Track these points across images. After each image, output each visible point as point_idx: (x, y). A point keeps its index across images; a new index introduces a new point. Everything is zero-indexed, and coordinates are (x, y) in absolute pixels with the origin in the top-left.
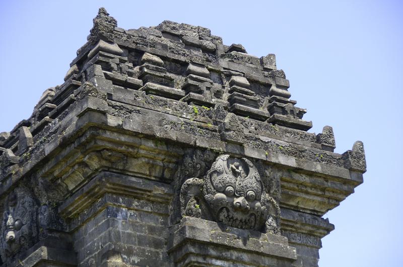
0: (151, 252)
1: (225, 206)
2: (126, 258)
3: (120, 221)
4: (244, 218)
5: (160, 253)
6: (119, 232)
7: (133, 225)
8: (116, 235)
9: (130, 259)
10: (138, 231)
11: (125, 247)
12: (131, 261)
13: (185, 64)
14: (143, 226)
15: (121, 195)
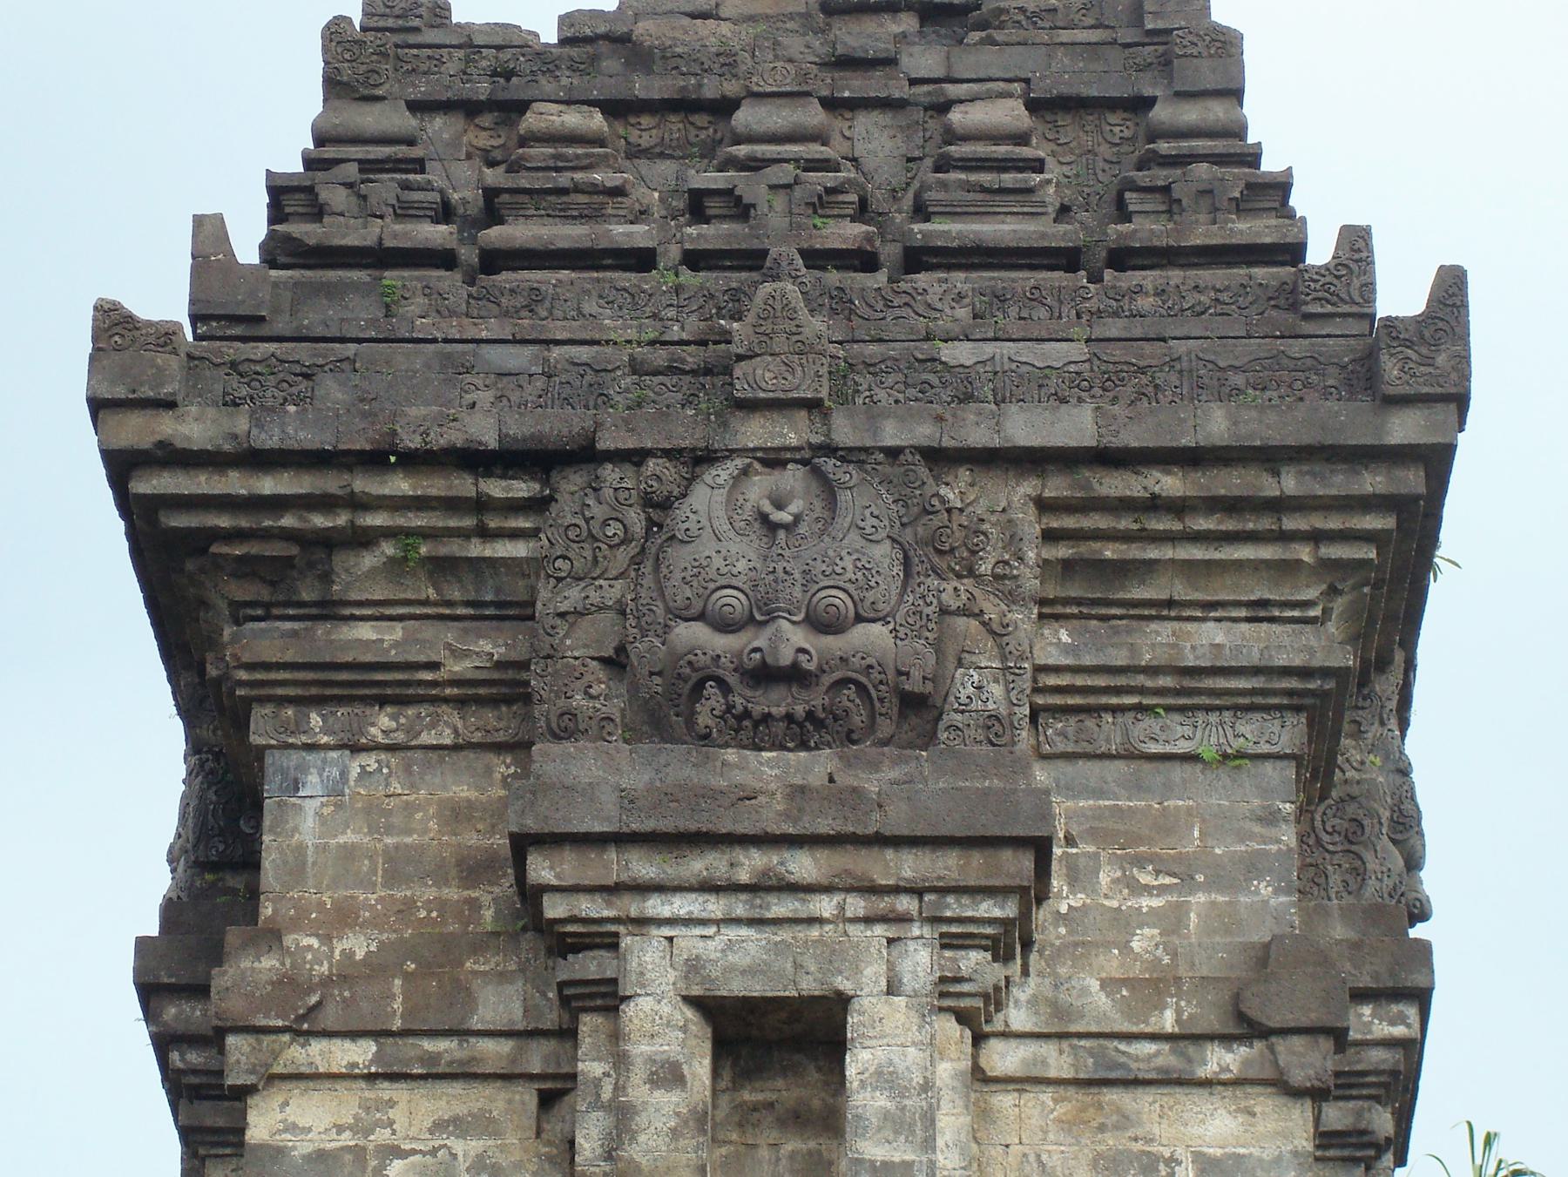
0: (441, 904)
2: (316, 946)
3: (311, 806)
4: (800, 710)
5: (486, 899)
6: (301, 849)
7: (375, 815)
8: (285, 863)
9: (332, 951)
10: (389, 830)
11: (322, 904)
12: (337, 952)
13: (725, 107)
14: (419, 808)
15: (319, 701)
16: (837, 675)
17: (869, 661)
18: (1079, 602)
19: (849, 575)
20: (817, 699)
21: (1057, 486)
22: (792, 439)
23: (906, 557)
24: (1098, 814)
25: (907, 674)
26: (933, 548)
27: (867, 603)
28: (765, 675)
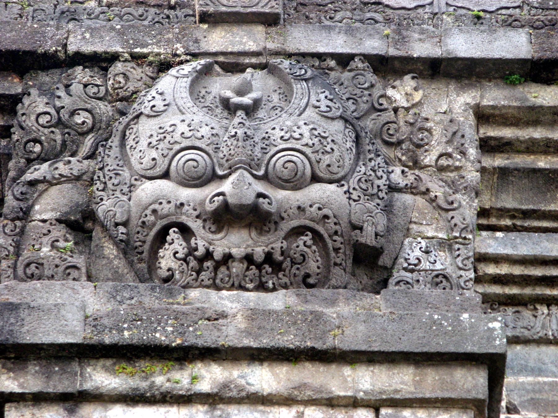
1: (173, 219)
4: (259, 252)
16: (295, 223)
17: (325, 211)
18: (512, 214)
19: (305, 140)
20: (274, 242)
21: (494, 96)
22: (252, 46)
23: (358, 137)
24: (539, 388)
25: (361, 229)
26: (378, 136)
27: (323, 165)
28: (225, 217)
